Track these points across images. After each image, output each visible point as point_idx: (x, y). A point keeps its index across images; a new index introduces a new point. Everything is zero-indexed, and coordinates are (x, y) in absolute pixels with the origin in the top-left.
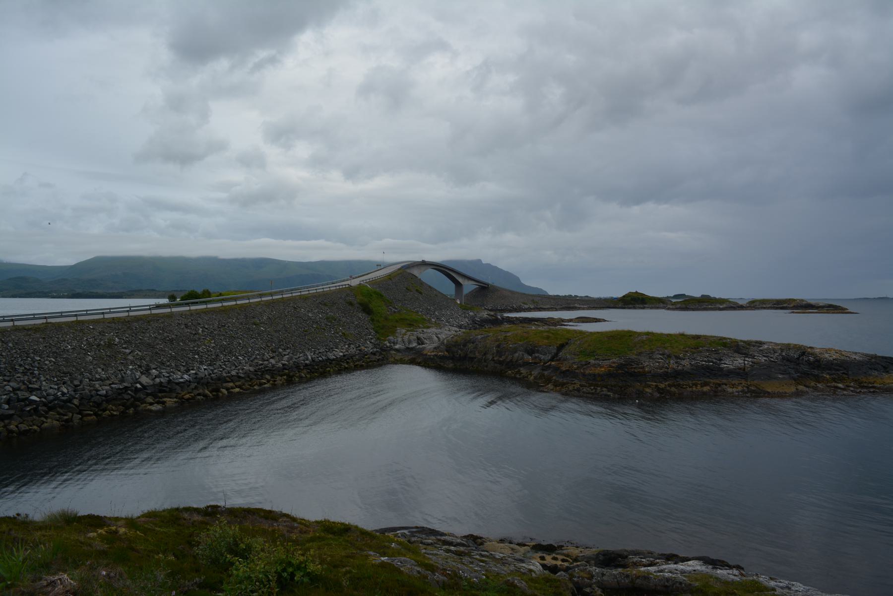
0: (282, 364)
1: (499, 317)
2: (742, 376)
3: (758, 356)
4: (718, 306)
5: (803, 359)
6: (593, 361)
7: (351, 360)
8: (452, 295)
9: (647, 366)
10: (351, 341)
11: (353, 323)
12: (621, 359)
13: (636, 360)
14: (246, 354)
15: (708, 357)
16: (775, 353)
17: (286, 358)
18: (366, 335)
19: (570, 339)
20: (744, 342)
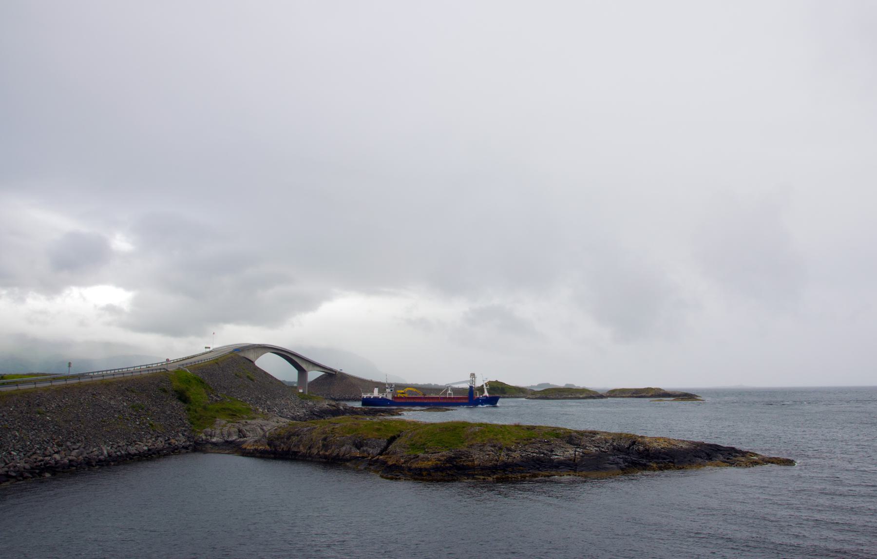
0: (68, 459)
1: (341, 408)
2: (571, 467)
3: (589, 447)
4: (578, 395)
5: (633, 448)
6: (422, 455)
7: (157, 454)
8: (295, 383)
9: (476, 459)
10: (160, 433)
11: (164, 413)
12: (451, 452)
13: (466, 453)
14: (22, 448)
15: (539, 448)
16: (606, 442)
17: (74, 453)
18: (179, 426)
19: (403, 431)
20: (577, 432)
